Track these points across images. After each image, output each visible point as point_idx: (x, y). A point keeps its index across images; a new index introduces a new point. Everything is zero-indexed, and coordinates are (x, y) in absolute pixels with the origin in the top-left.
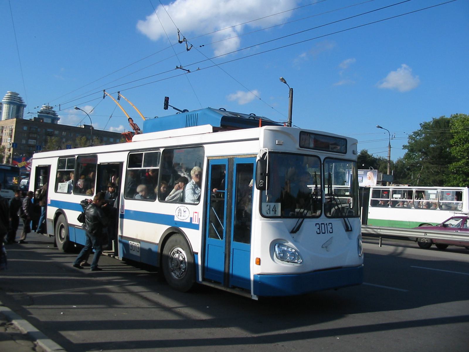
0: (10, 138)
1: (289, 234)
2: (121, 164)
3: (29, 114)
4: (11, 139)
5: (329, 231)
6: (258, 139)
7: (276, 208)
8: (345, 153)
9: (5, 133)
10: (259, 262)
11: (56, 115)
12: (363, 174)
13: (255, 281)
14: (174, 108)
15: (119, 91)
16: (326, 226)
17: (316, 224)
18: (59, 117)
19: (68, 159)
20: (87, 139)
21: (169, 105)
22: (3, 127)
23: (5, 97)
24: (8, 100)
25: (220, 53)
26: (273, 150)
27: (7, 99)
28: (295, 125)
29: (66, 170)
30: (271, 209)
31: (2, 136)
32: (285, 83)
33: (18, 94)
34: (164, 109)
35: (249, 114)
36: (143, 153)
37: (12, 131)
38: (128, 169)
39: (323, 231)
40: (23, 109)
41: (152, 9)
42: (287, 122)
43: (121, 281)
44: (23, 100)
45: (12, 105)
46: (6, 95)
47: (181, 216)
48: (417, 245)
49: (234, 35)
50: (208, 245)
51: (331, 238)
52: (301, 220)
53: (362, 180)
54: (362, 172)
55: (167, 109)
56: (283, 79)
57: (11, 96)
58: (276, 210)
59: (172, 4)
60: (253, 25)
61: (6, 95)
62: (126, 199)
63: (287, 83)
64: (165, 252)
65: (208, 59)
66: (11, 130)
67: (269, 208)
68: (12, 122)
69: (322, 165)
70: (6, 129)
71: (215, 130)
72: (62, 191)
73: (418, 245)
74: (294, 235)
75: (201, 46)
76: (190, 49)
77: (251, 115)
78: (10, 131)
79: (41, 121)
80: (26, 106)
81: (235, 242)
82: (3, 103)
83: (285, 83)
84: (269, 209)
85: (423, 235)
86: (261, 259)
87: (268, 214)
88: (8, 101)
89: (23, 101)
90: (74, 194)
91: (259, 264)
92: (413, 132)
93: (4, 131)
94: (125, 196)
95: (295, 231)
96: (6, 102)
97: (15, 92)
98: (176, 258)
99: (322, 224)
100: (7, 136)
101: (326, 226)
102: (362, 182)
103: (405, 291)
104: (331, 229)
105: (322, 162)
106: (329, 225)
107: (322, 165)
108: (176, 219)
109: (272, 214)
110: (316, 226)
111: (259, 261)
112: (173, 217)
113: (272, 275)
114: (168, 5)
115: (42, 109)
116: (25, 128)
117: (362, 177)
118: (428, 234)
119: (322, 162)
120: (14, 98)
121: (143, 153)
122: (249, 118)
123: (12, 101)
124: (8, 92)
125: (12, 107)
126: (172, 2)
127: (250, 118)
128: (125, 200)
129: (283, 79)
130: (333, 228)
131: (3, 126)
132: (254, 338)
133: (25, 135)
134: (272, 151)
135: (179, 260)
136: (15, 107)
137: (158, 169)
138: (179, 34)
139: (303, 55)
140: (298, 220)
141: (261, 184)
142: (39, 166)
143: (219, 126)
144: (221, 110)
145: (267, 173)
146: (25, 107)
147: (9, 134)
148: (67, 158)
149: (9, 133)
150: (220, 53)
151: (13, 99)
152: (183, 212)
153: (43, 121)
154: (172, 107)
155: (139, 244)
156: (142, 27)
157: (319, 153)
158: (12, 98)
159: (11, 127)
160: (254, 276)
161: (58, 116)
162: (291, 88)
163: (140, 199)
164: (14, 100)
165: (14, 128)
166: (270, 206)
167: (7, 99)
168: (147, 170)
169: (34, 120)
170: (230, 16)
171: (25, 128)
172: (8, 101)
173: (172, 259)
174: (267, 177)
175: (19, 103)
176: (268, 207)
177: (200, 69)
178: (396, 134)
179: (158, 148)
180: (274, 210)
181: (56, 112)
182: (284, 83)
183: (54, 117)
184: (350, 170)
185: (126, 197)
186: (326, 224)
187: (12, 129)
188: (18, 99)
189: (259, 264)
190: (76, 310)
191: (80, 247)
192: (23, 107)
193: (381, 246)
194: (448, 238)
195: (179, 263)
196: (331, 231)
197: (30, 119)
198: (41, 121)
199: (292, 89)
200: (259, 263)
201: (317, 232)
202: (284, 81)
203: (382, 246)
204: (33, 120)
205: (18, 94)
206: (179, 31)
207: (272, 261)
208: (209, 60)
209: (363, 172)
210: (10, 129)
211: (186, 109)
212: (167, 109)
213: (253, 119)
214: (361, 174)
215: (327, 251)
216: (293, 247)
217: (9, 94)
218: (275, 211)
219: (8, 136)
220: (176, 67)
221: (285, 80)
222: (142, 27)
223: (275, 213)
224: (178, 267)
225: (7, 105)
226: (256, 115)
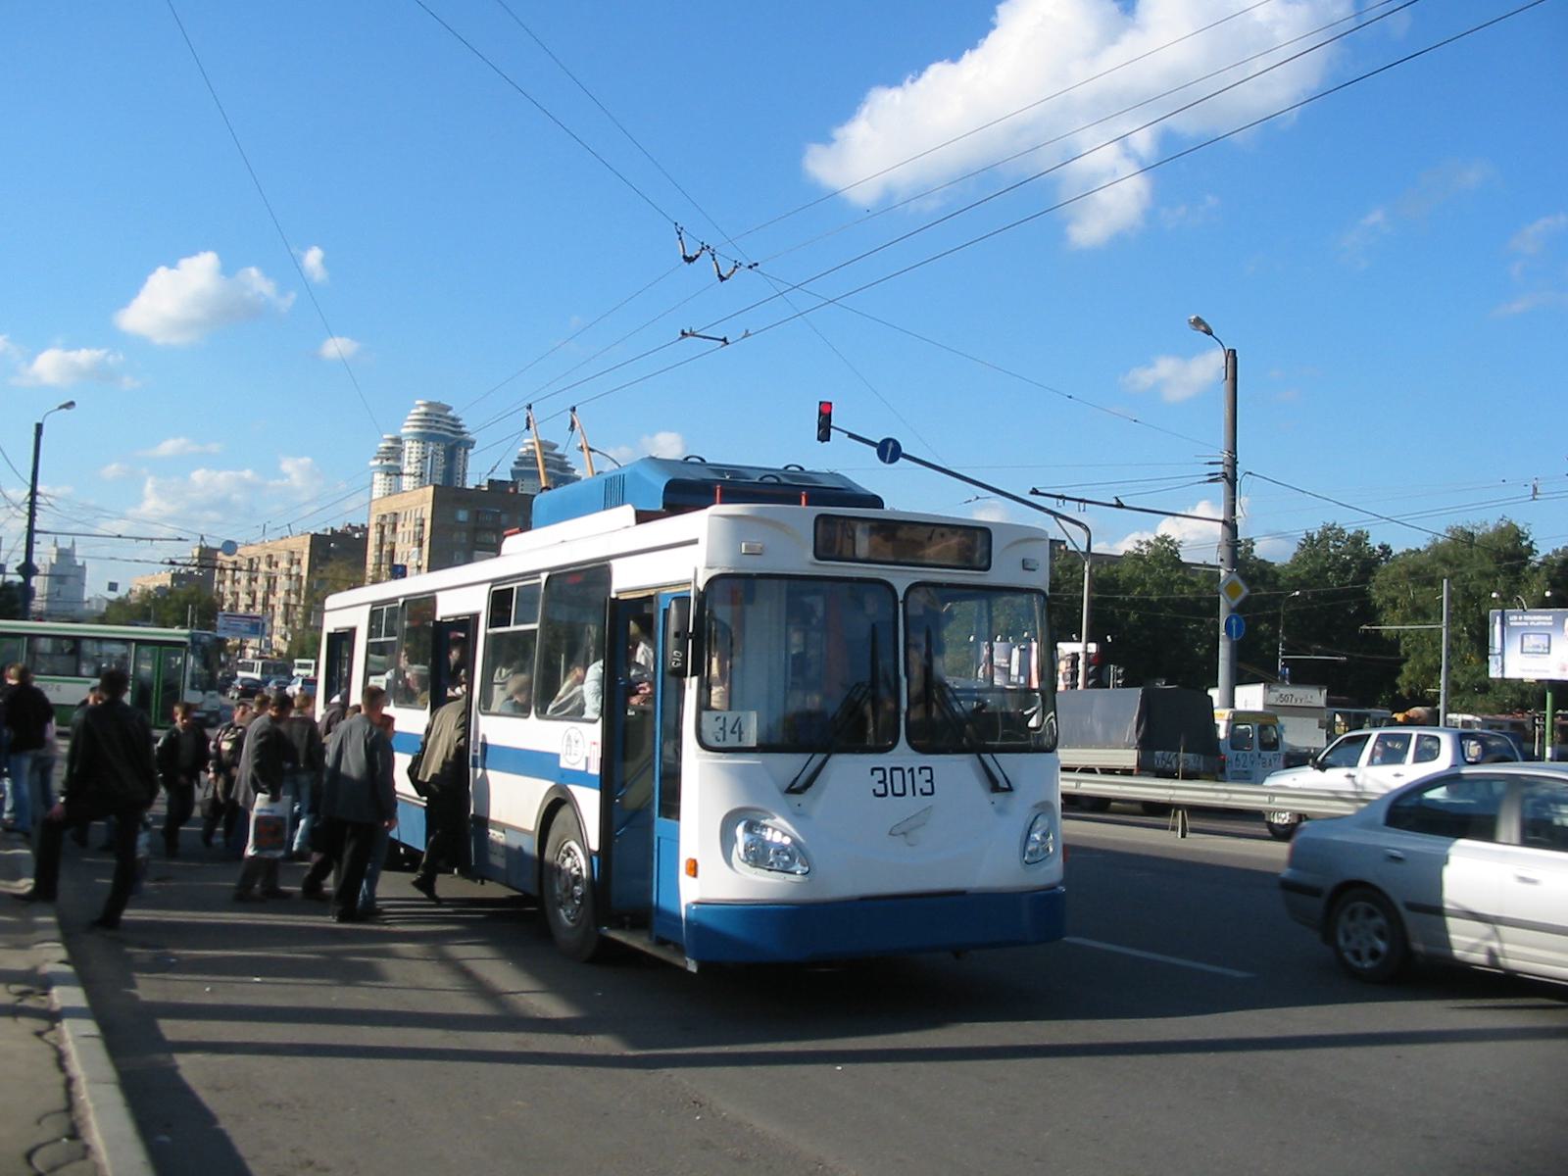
0: (416, 549)
1: (779, 795)
2: (475, 617)
3: (476, 474)
4: (420, 552)
5: (921, 790)
6: (695, 542)
7: (742, 726)
8: (987, 568)
9: (404, 533)
10: (693, 869)
11: (569, 468)
12: (1551, 624)
13: (688, 921)
14: (851, 436)
15: (574, 405)
16: (908, 776)
17: (873, 770)
18: (576, 473)
19: (387, 609)
20: (76, 576)
21: (836, 428)
22: (396, 514)
23: (410, 418)
24: (420, 427)
25: (1088, 231)
26: (735, 568)
27: (415, 426)
28: (1249, 471)
29: (382, 639)
30: (728, 729)
31: (394, 543)
32: (1209, 332)
33: (449, 409)
34: (819, 439)
35: (781, 467)
36: (512, 589)
37: (422, 525)
38: (490, 631)
39: (899, 789)
40: (466, 453)
41: (844, 106)
42: (1221, 460)
44: (464, 426)
45: (431, 443)
46: (413, 411)
47: (570, 754)
48: (1266, 831)
49: (1128, 167)
50: (659, 839)
51: (926, 809)
52: (819, 758)
53: (1549, 648)
54: (1546, 618)
55: (829, 440)
56: (1198, 322)
57: (426, 414)
58: (742, 729)
59: (913, 81)
60: (1188, 125)
61: (413, 411)
62: (483, 714)
64: (548, 855)
66: (418, 522)
67: (722, 726)
68: (424, 498)
69: (901, 606)
70: (405, 519)
71: (642, 517)
73: (1267, 830)
74: (796, 798)
75: (750, 267)
76: (729, 275)
77: (790, 469)
78: (416, 525)
79: (511, 490)
80: (474, 443)
81: (662, 819)
82: (403, 439)
83: (1209, 332)
84: (721, 729)
85: (1264, 802)
86: (698, 862)
87: (719, 741)
88: (417, 430)
89: (463, 429)
90: (396, 706)
91: (695, 876)
93: (399, 528)
94: (482, 706)
95: (796, 788)
96: (411, 434)
97: (439, 403)
98: (565, 870)
99: (892, 769)
100: (409, 542)
101: (908, 776)
102: (1549, 653)
103: (1238, 974)
105: (901, 598)
106: (920, 773)
107: (901, 606)
108: (563, 764)
109: (732, 741)
110: (872, 774)
111: (693, 865)
112: (556, 757)
113: (705, 906)
114: (901, 85)
115: (524, 449)
116: (462, 515)
117: (1546, 637)
118: (1277, 799)
119: (901, 598)
120: (437, 422)
121: (512, 589)
122: (761, 479)
123: (430, 431)
124: (418, 402)
125: (431, 448)
126: (911, 76)
127: (766, 479)
128: (481, 717)
129: (1198, 322)
130: (934, 781)
131: (398, 511)
132: (628, 1057)
133: (464, 535)
134: (732, 571)
135: (571, 874)
137: (535, 631)
138: (680, 239)
139: (1376, 217)
140: (811, 758)
141: (677, 662)
142: (336, 629)
143: (660, 507)
144: (692, 463)
145: (691, 630)
146: (472, 448)
147: (414, 537)
148: (385, 607)
149: (415, 533)
150: (1088, 231)
151: (433, 424)
152: (574, 743)
153: (516, 490)
154: (846, 432)
155: (502, 835)
156: (826, 167)
157: (883, 572)
158: (431, 420)
159: (418, 516)
160: (687, 907)
161: (574, 470)
162: (1229, 350)
163: (509, 711)
164: (439, 429)
165: (429, 515)
166: (725, 719)
167: (415, 426)
169: (488, 487)
170: (1109, 107)
171: (462, 515)
172: (417, 430)
173: (559, 871)
174: (690, 642)
176: (720, 723)
177: (750, 332)
178: (1507, 482)
179: (536, 573)
180: (736, 729)
181: (566, 460)
182: (1205, 335)
183: (562, 476)
184: (1506, 611)
185: (485, 709)
186: (911, 770)
187: (423, 520)
188: (448, 424)
189: (695, 876)
190: (258, 986)
191: (413, 854)
193: (1183, 836)
194: (1202, 798)
195: (570, 881)
196: (927, 788)
197: (477, 486)
198: (511, 490)
199: (1234, 351)
200: (693, 873)
201: (874, 791)
202: (1203, 328)
203: (1188, 835)
204: (486, 489)
205: (449, 409)
206: (682, 229)
207: (725, 865)
209: (1550, 618)
210: (416, 519)
211: (890, 436)
212: (829, 440)
213: (775, 481)
214: (1544, 624)
215: (911, 845)
216: (786, 829)
217: (423, 409)
218: (741, 733)
219: (411, 544)
220: (680, 332)
221: (1204, 323)
222: (826, 167)
223: (740, 740)
224: (569, 894)
225: (415, 445)
226: (806, 469)
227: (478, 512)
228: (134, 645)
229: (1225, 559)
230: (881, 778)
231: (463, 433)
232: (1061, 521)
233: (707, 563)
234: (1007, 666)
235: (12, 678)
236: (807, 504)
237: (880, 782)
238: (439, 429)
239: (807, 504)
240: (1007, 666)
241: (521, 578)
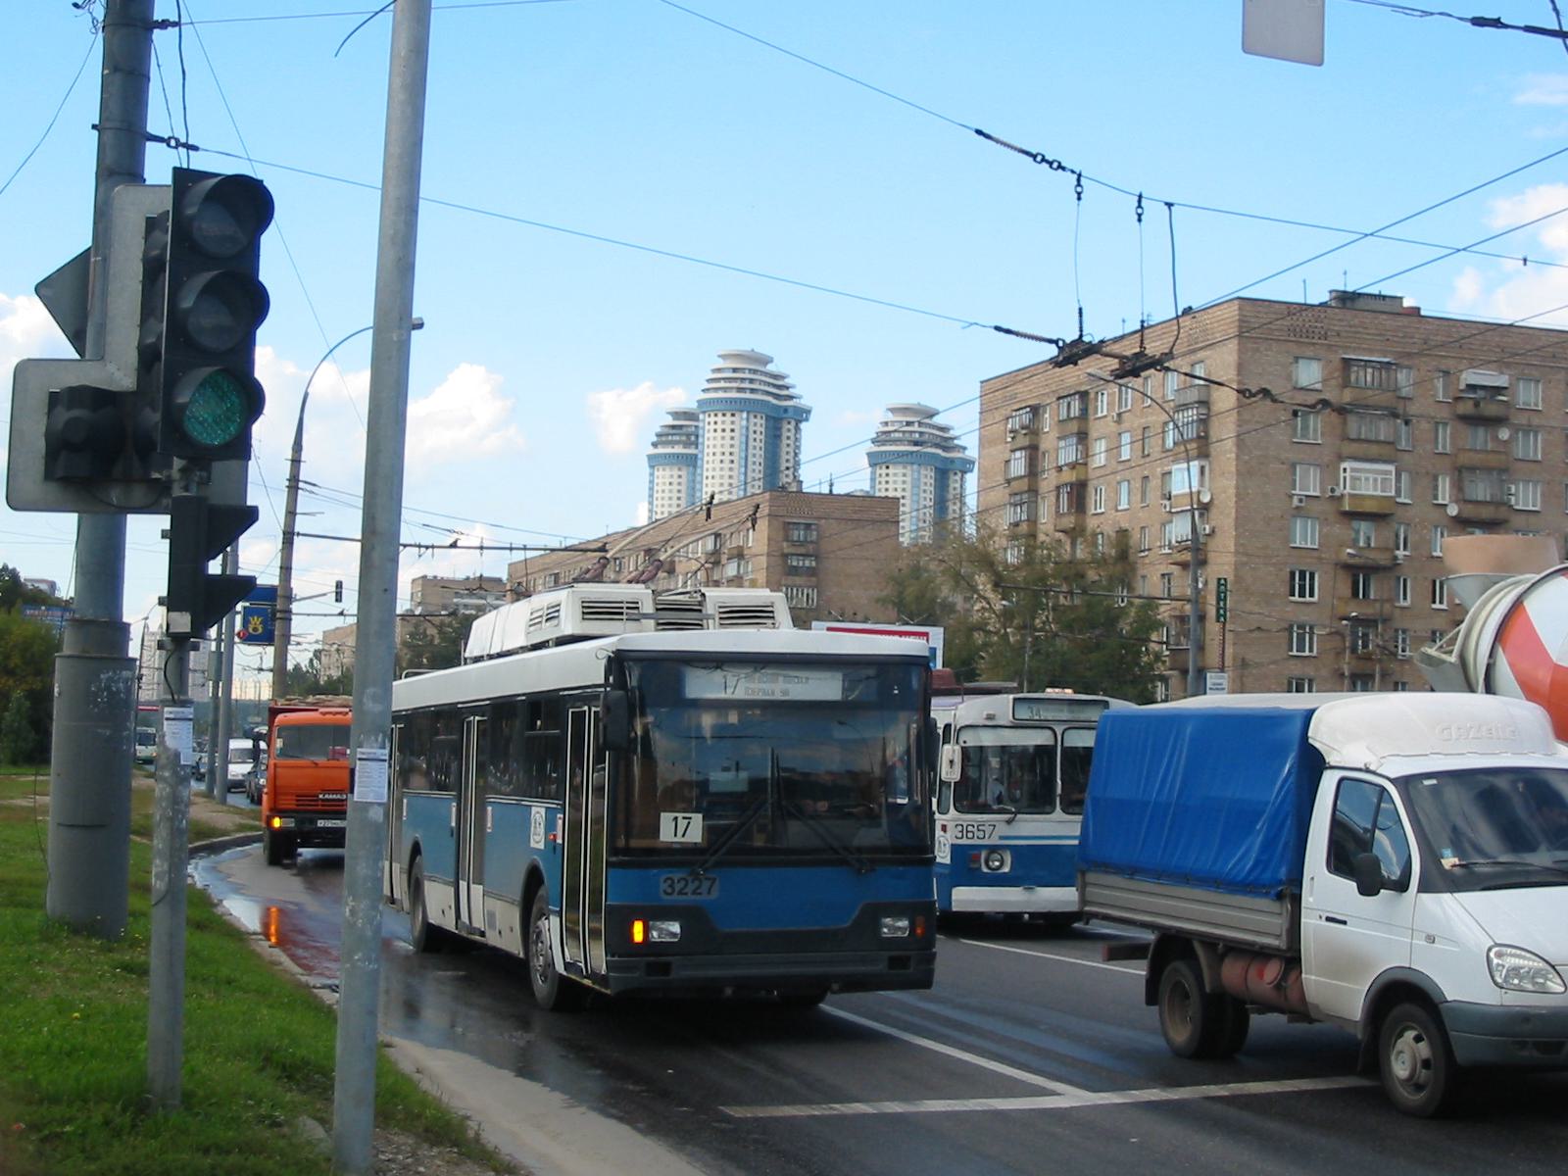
11: (957, 446)
33: (767, 360)
40: (797, 429)
43: (877, 1021)
63: (1469, 24)
65: (254, 163)
72: (1466, 818)
80: (808, 412)
89: (791, 392)
92: (668, 413)
120: (751, 381)
136: (759, 424)
146: (807, 420)
151: (746, 385)
158: (743, 380)
168: (1359, 688)
175: (775, 401)
188: (769, 384)
192: (798, 422)
208: (248, 161)
227: (1347, 363)
228: (558, 909)
229: (1139, 578)
231: (791, 397)
232: (1473, 249)
233: (1171, 477)
234: (1159, 699)
235: (646, 931)
236: (342, 846)
238: (753, 391)
239: (342, 846)
240: (1159, 699)
241: (621, 817)
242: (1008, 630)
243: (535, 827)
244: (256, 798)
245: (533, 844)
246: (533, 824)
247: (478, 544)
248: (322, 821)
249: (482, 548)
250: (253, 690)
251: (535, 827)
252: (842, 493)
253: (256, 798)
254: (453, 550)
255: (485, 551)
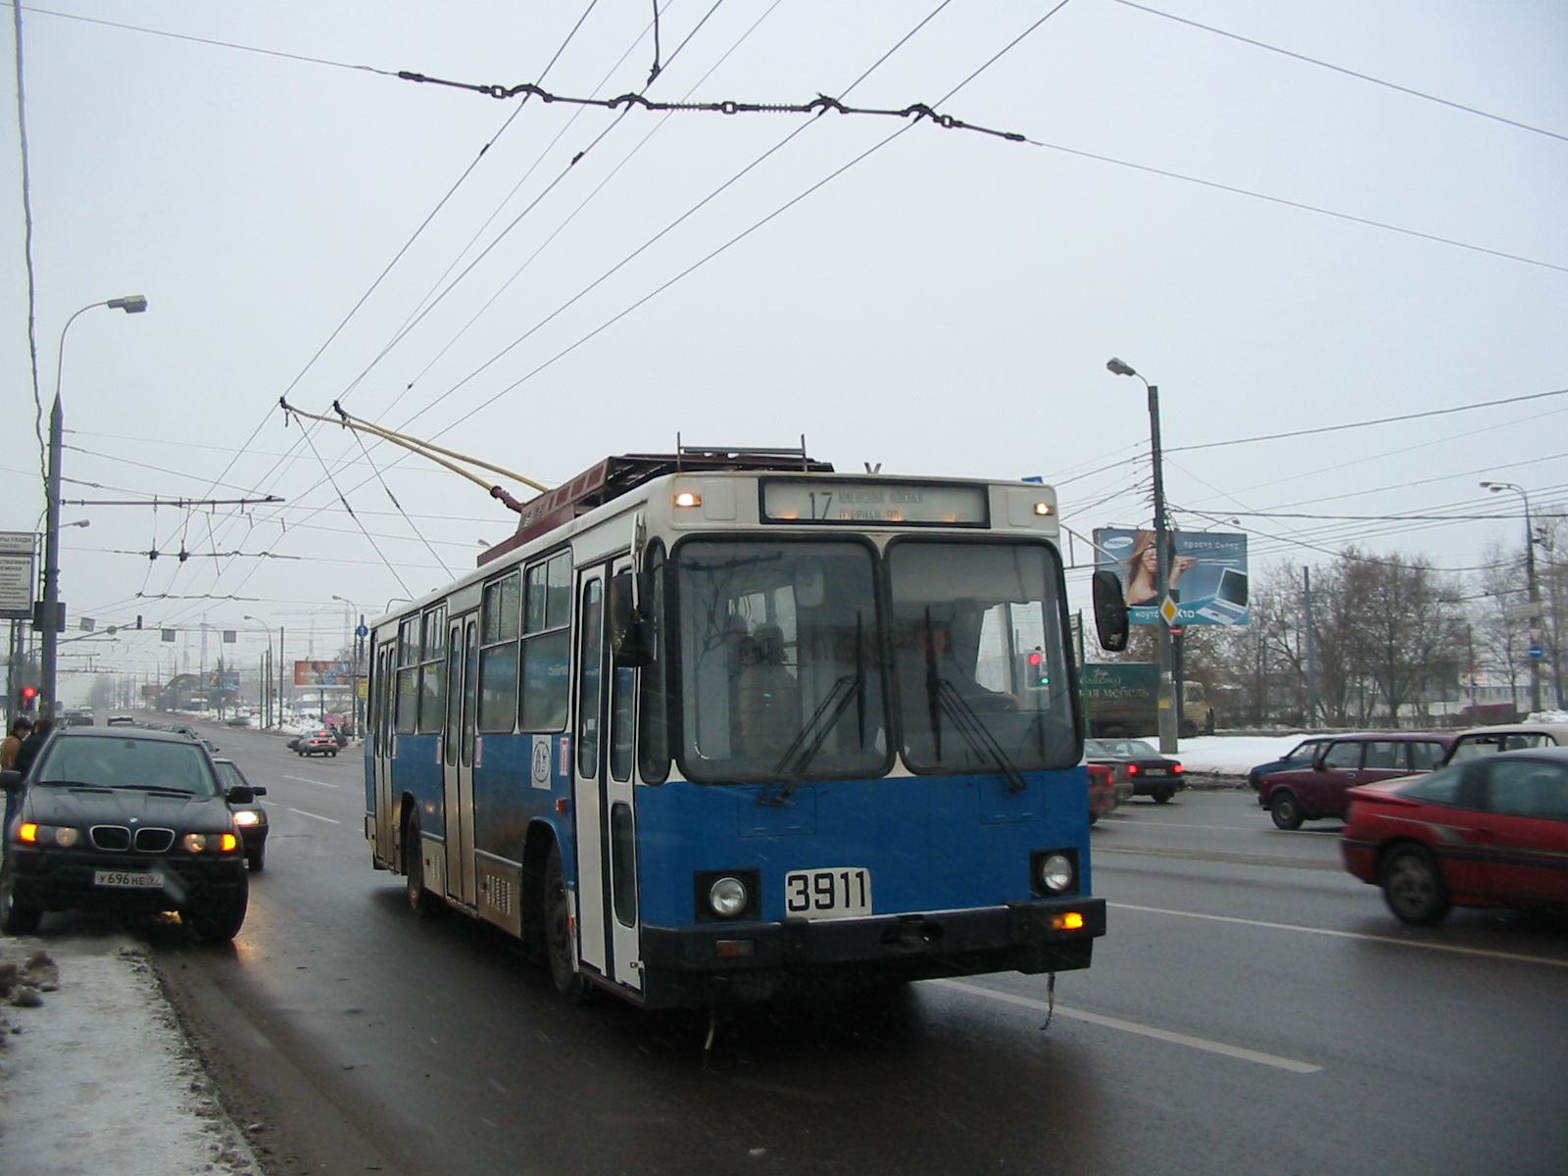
5: (790, 901)
104: (803, 896)
106: (790, 884)
230: (802, 888)
237: (798, 893)
242: (1388, 643)
243: (538, 762)
244: (66, 1065)
245: (535, 784)
246: (535, 759)
247: (152, 499)
248: (107, 874)
249: (155, 503)
250: (273, 673)
251: (538, 762)
252: (46, 499)
253: (66, 1065)
254: (269, 503)
255: (158, 506)
